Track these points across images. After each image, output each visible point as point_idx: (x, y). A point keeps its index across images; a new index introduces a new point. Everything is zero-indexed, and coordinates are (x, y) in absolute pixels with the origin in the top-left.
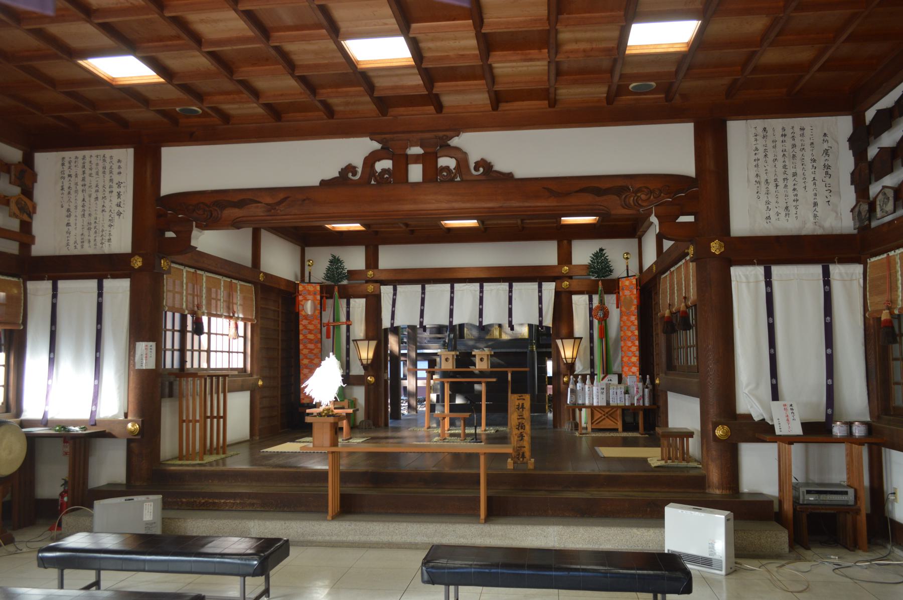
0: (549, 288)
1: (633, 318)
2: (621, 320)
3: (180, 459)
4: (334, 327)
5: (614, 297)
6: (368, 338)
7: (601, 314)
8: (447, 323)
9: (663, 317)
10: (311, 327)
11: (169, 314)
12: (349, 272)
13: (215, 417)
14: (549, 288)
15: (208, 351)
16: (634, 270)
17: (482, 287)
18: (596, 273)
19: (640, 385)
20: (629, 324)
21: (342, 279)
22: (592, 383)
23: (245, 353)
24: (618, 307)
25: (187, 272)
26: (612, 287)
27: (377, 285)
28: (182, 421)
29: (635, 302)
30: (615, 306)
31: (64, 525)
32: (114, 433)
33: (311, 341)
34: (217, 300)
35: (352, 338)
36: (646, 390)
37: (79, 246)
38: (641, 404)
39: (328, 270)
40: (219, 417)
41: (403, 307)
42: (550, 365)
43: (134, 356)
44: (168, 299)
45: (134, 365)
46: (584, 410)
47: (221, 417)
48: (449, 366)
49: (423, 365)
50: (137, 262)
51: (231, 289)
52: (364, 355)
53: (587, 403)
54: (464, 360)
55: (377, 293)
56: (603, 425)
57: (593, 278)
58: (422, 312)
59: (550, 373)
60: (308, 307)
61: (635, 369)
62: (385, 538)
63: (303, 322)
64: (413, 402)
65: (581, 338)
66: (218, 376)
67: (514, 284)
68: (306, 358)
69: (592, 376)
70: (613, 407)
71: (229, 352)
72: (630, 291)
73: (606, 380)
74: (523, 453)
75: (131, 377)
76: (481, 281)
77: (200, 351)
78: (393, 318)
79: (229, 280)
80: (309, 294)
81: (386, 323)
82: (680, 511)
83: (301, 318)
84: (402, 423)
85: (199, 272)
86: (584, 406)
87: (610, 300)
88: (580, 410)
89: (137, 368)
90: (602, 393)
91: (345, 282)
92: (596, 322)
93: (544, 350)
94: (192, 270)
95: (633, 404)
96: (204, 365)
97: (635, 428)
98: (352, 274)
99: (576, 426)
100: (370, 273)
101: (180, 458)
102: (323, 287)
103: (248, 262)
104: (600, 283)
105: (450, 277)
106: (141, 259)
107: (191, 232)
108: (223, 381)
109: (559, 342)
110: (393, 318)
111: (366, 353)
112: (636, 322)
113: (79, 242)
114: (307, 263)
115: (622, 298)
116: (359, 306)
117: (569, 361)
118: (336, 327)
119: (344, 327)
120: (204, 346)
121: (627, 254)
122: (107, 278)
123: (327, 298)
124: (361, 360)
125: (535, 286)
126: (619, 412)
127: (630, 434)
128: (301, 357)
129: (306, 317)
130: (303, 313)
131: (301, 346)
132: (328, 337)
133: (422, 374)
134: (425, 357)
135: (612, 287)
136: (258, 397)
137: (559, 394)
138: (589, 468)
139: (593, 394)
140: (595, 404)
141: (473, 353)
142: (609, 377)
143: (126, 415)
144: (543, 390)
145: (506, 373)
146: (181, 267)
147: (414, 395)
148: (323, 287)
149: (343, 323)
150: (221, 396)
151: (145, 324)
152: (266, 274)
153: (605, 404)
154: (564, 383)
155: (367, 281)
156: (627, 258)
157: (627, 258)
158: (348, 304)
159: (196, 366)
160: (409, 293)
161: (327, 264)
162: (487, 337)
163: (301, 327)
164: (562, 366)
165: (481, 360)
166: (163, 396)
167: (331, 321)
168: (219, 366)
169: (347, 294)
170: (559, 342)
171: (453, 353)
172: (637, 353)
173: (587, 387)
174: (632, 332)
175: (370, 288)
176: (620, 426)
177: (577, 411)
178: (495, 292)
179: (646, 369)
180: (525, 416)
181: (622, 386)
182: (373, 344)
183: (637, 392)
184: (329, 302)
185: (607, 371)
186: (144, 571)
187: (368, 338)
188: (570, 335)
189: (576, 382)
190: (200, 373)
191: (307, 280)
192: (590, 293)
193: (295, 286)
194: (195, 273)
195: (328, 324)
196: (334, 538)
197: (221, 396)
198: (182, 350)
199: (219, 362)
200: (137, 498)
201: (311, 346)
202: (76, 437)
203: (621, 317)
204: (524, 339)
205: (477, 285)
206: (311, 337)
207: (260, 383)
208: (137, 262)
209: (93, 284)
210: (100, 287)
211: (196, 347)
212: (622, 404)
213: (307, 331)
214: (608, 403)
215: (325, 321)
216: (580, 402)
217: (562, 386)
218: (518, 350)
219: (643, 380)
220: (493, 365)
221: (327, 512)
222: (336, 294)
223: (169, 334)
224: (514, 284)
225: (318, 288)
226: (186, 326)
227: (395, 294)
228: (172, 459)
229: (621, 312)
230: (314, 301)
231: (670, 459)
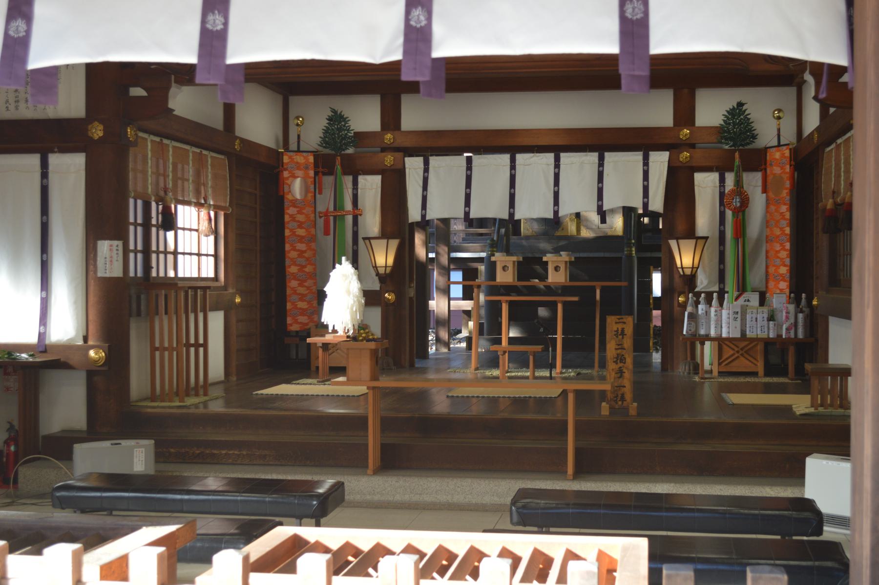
0: (660, 161)
1: (784, 208)
2: (767, 211)
3: (153, 401)
4: (335, 217)
5: (758, 176)
6: (385, 234)
7: (737, 202)
8: (506, 216)
9: (824, 209)
10: (301, 218)
11: (131, 201)
12: (357, 134)
13: (192, 345)
14: (660, 161)
15: (175, 253)
16: (789, 135)
17: (557, 160)
18: (731, 139)
19: (792, 307)
20: (777, 216)
21: (347, 145)
22: (721, 304)
23: (216, 256)
24: (764, 190)
25: (152, 141)
26: (756, 160)
27: (399, 155)
28: (154, 349)
29: (788, 184)
30: (760, 189)
31: (21, 479)
32: (71, 362)
33: (301, 239)
34: (184, 180)
35: (361, 235)
36: (800, 316)
37: (12, 107)
38: (792, 335)
39: (326, 131)
40: (197, 345)
41: (440, 190)
42: (657, 279)
43: (95, 260)
44: (134, 182)
45: (95, 272)
46: (708, 344)
47: (201, 345)
48: (505, 277)
49: (457, 276)
50: (97, 131)
51: (200, 161)
52: (380, 260)
53: (713, 333)
54: (530, 267)
55: (400, 166)
56: (735, 367)
57: (727, 147)
58: (468, 197)
59: (657, 290)
60: (297, 188)
61: (784, 285)
62: (443, 498)
63: (291, 211)
64: (444, 335)
65: (706, 238)
66: (195, 289)
67: (607, 154)
68: (295, 264)
69: (722, 294)
70: (752, 340)
71: (199, 255)
72: (780, 166)
73: (741, 301)
74: (623, 395)
75: (92, 288)
76: (557, 150)
77: (166, 253)
78: (424, 206)
79: (198, 150)
80: (299, 168)
81: (414, 214)
82: (824, 462)
83: (286, 204)
84: (430, 363)
85: (166, 141)
86: (707, 337)
87: (753, 181)
88: (703, 344)
89: (100, 274)
90: (735, 319)
91: (350, 151)
92: (729, 214)
93: (648, 255)
94: (157, 139)
95: (780, 336)
96: (171, 274)
97: (784, 373)
98: (361, 138)
99: (696, 368)
100: (389, 136)
101: (153, 398)
102: (316, 155)
103: (219, 125)
104: (737, 155)
105: (510, 144)
106: (101, 127)
107: (168, 88)
108: (196, 293)
109: (673, 243)
110: (424, 206)
111: (384, 257)
112: (788, 215)
113: (12, 100)
114: (292, 123)
115: (770, 178)
116: (371, 186)
117: (688, 272)
118: (339, 218)
119: (349, 219)
120: (171, 247)
121: (780, 111)
122: (53, 152)
123: (324, 174)
124: (375, 267)
125: (638, 156)
126: (760, 347)
127: (775, 380)
128: (288, 262)
129: (294, 203)
130: (290, 197)
131: (287, 247)
132: (327, 233)
133: (457, 291)
134: (461, 264)
135: (756, 160)
136: (233, 319)
137: (672, 321)
138: (709, 416)
139: (721, 321)
140: (724, 335)
141: (545, 259)
142: (746, 295)
143: (85, 339)
144: (644, 318)
145: (593, 289)
146: (145, 135)
147: (443, 323)
148: (316, 155)
149: (348, 213)
150: (201, 316)
151: (104, 217)
152: (244, 141)
153: (738, 335)
154: (679, 305)
155: (384, 150)
156: (779, 118)
157: (779, 118)
158: (355, 183)
159: (162, 274)
160: (447, 169)
161: (325, 123)
162: (558, 233)
163: (287, 218)
164: (677, 280)
165: (557, 269)
166: (130, 315)
167: (331, 209)
168: (188, 275)
169: (354, 170)
170: (673, 243)
171: (515, 258)
172: (788, 261)
173: (713, 310)
174: (782, 229)
175: (389, 159)
176: (760, 368)
177: (698, 346)
178: (578, 166)
179: (801, 284)
180: (625, 346)
181: (765, 309)
182: (394, 244)
183: (787, 317)
184: (328, 180)
185: (742, 288)
186: (182, 511)
187: (385, 234)
188: (690, 233)
189: (697, 303)
190: (180, 284)
191: (293, 146)
192: (722, 170)
193: (278, 156)
194: (161, 143)
195: (326, 214)
196: (377, 498)
197: (201, 316)
198: (147, 252)
199: (187, 268)
200: (125, 443)
201: (302, 247)
202: (25, 365)
203: (767, 206)
204: (618, 237)
205: (551, 157)
206: (301, 232)
207: (238, 300)
208: (97, 131)
209: (33, 161)
210: (44, 165)
211: (162, 248)
212: (765, 335)
213: (295, 224)
214: (743, 333)
215: (321, 208)
216: (702, 332)
217: (677, 309)
218: (607, 255)
219: (797, 301)
220: (572, 278)
221: (367, 467)
222: (339, 168)
223: (132, 228)
224: (607, 154)
225: (311, 159)
226: (150, 218)
227: (426, 170)
228: (137, 401)
229: (768, 199)
230: (305, 179)
231: (822, 405)
